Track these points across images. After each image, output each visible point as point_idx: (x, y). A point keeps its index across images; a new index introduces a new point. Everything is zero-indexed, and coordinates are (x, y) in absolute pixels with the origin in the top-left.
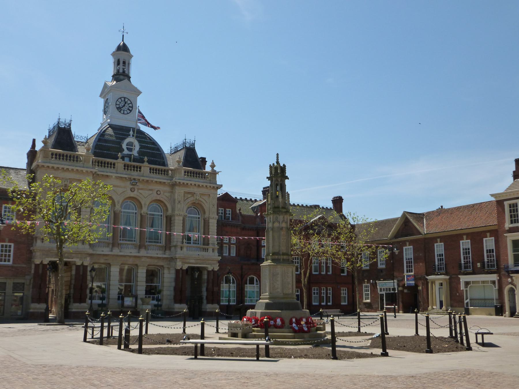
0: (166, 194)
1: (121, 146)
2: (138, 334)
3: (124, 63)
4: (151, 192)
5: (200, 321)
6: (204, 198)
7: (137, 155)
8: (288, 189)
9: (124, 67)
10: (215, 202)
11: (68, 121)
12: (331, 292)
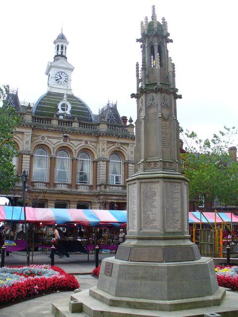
2: (99, 255)
3: (62, 47)
7: (69, 113)
8: (180, 118)
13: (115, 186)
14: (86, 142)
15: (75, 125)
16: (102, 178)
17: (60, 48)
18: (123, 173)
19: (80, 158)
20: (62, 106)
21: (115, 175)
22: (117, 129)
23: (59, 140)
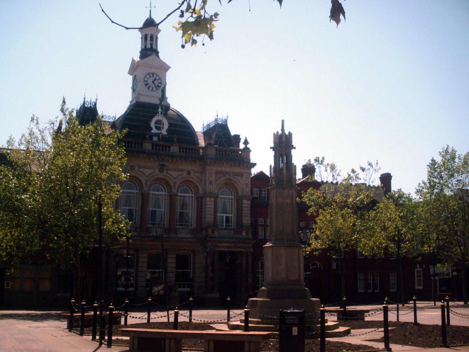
0: (197, 174)
1: (149, 125)
3: (152, 37)
4: (180, 173)
5: (243, 309)
6: (237, 177)
7: (166, 133)
9: (152, 42)
10: (249, 182)
11: (93, 100)
12: (378, 278)
13: (226, 229)
14: (189, 173)
15: (175, 149)
16: (209, 218)
17: (149, 38)
18: (235, 212)
19: (180, 193)
20: (156, 123)
21: (225, 215)
22: (228, 155)
23: (153, 171)
